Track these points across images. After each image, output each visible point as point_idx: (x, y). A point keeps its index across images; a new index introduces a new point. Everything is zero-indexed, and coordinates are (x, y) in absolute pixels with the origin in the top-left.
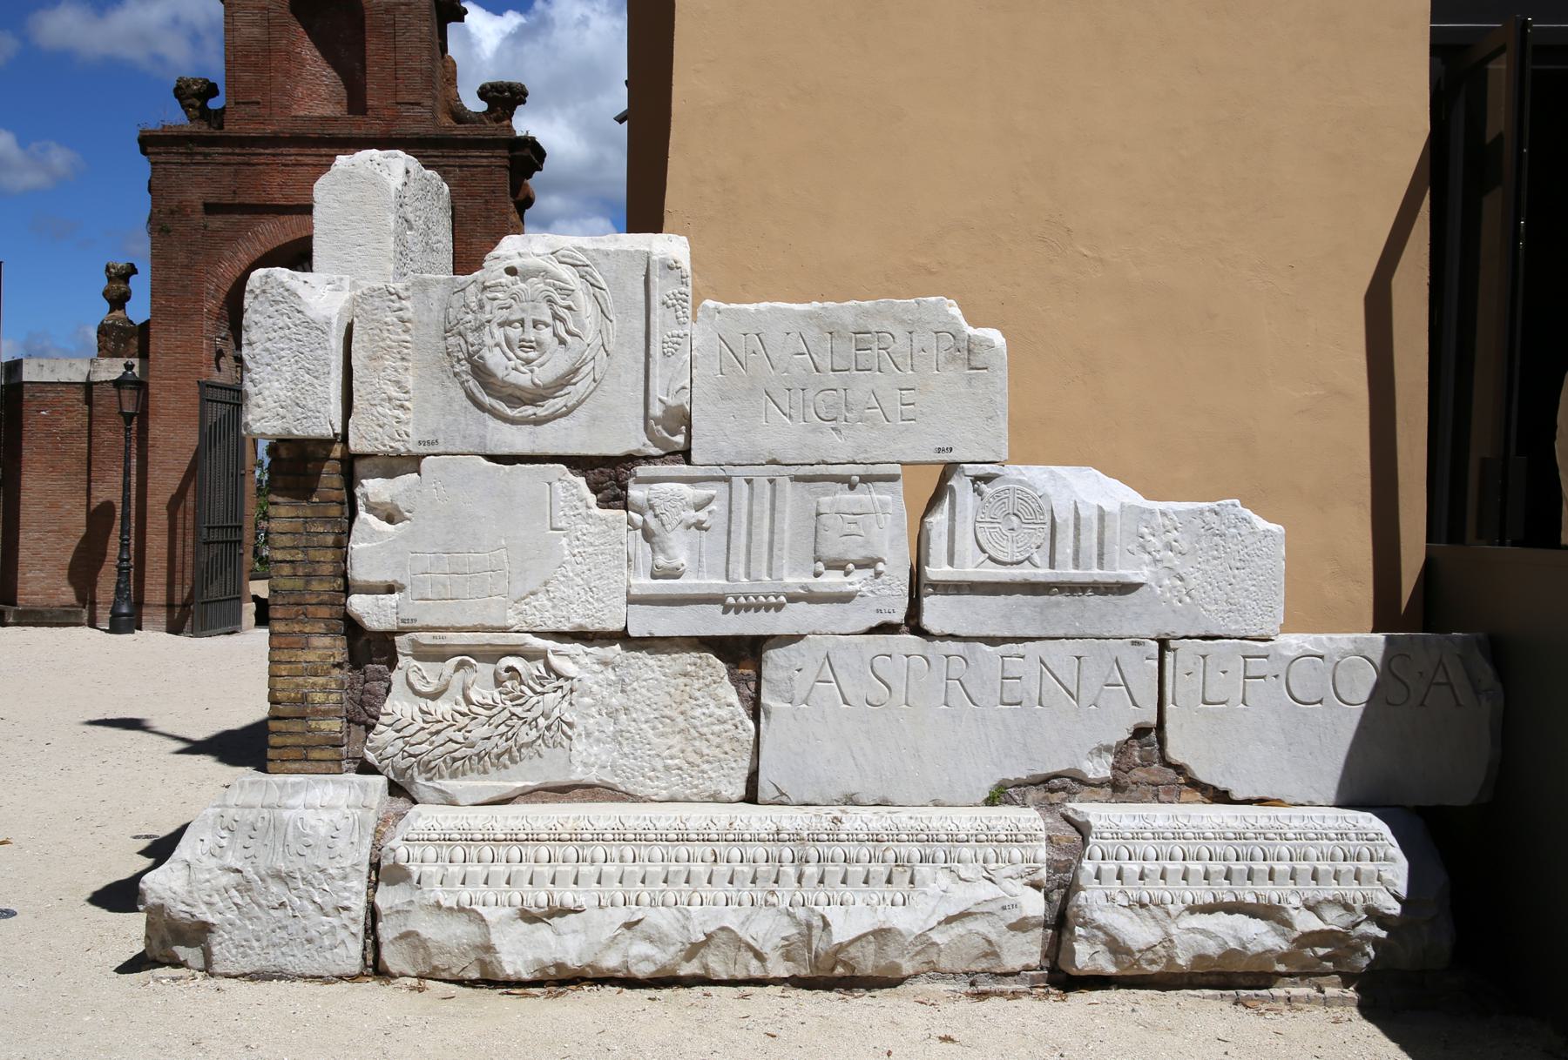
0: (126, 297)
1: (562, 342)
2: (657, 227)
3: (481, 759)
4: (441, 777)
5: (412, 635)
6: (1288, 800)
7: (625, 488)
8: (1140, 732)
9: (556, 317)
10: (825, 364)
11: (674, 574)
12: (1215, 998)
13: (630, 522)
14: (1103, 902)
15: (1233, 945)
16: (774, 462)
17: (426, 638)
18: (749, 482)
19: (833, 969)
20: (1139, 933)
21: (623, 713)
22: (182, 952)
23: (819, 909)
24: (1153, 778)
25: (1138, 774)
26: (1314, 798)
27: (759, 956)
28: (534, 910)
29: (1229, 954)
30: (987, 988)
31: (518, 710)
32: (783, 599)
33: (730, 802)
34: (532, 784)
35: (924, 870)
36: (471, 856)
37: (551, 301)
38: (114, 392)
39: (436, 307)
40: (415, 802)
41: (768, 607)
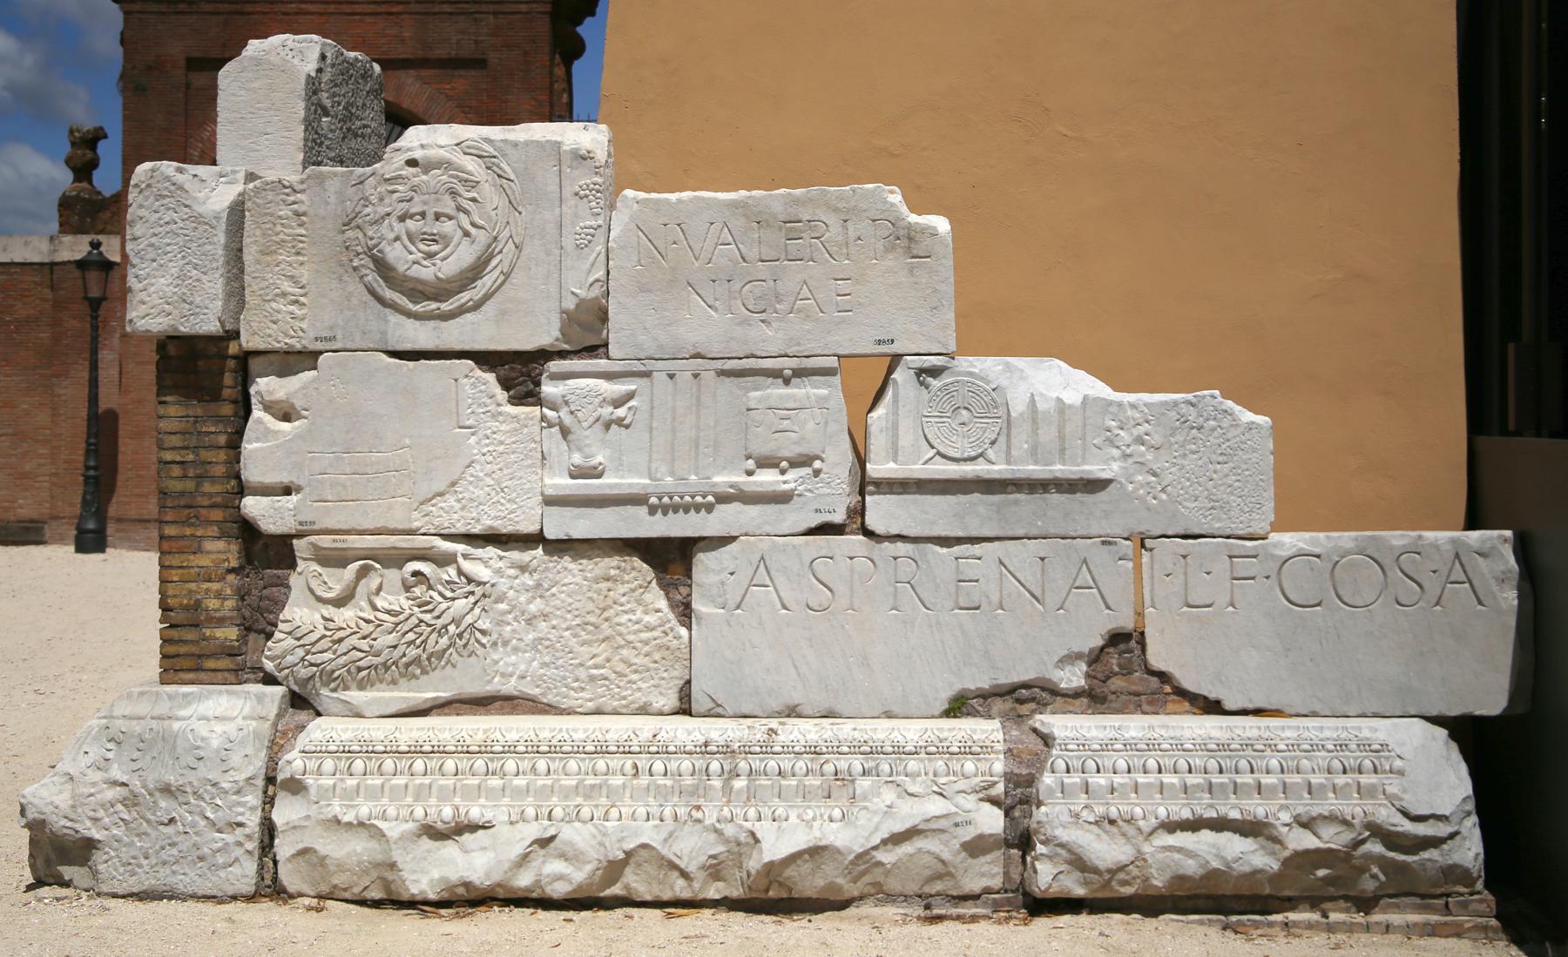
0: (94, 164)
1: (467, 234)
2: (567, 115)
3: (387, 669)
4: (346, 688)
5: (313, 538)
6: (1288, 710)
7: (538, 384)
8: (1117, 639)
9: (459, 208)
10: (752, 254)
11: (594, 473)
12: (1201, 923)
13: (543, 418)
14: (1066, 818)
15: (1215, 864)
16: (697, 356)
17: (326, 541)
18: (671, 376)
19: (767, 891)
20: (1106, 851)
21: (543, 618)
22: (67, 872)
23: (748, 825)
24: (1134, 688)
25: (1117, 683)
26: (1318, 707)
27: (684, 875)
28: (439, 825)
29: (1213, 875)
30: (943, 912)
31: (427, 617)
32: (710, 498)
33: (661, 714)
34: (444, 695)
35: (864, 784)
36: (369, 771)
37: (454, 193)
38: (78, 273)
39: (333, 199)
40: (319, 714)
41: (698, 507)
